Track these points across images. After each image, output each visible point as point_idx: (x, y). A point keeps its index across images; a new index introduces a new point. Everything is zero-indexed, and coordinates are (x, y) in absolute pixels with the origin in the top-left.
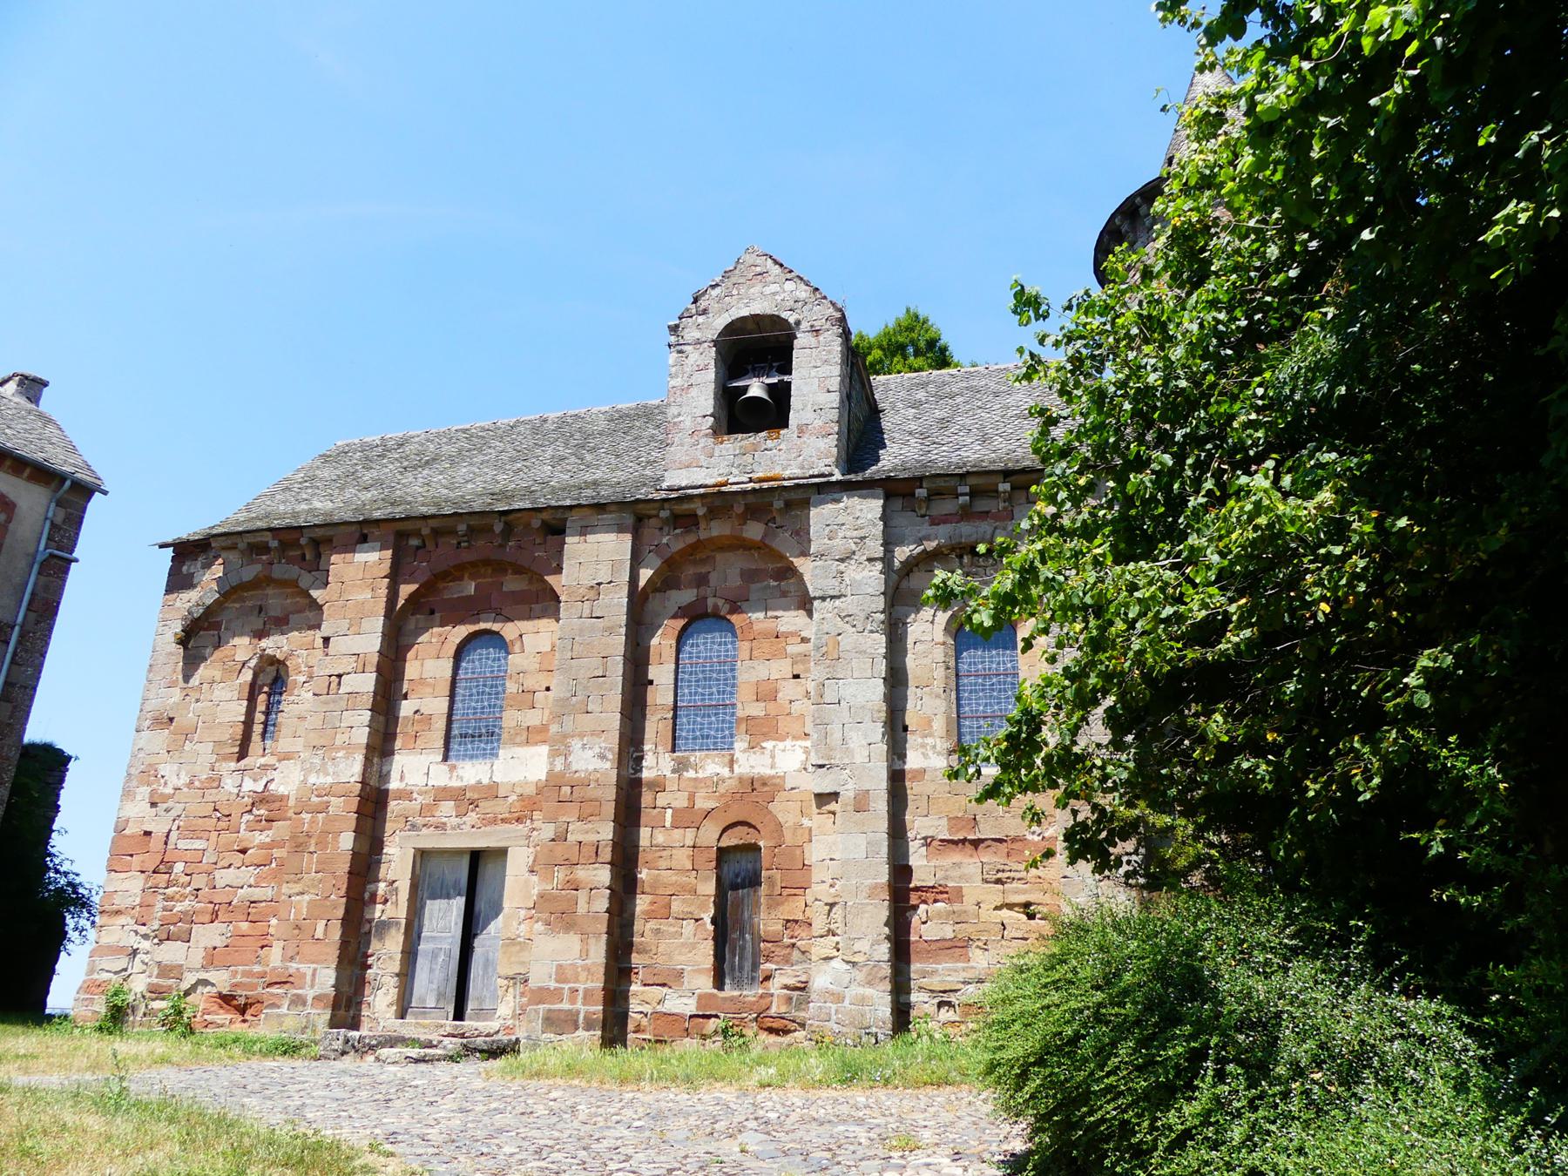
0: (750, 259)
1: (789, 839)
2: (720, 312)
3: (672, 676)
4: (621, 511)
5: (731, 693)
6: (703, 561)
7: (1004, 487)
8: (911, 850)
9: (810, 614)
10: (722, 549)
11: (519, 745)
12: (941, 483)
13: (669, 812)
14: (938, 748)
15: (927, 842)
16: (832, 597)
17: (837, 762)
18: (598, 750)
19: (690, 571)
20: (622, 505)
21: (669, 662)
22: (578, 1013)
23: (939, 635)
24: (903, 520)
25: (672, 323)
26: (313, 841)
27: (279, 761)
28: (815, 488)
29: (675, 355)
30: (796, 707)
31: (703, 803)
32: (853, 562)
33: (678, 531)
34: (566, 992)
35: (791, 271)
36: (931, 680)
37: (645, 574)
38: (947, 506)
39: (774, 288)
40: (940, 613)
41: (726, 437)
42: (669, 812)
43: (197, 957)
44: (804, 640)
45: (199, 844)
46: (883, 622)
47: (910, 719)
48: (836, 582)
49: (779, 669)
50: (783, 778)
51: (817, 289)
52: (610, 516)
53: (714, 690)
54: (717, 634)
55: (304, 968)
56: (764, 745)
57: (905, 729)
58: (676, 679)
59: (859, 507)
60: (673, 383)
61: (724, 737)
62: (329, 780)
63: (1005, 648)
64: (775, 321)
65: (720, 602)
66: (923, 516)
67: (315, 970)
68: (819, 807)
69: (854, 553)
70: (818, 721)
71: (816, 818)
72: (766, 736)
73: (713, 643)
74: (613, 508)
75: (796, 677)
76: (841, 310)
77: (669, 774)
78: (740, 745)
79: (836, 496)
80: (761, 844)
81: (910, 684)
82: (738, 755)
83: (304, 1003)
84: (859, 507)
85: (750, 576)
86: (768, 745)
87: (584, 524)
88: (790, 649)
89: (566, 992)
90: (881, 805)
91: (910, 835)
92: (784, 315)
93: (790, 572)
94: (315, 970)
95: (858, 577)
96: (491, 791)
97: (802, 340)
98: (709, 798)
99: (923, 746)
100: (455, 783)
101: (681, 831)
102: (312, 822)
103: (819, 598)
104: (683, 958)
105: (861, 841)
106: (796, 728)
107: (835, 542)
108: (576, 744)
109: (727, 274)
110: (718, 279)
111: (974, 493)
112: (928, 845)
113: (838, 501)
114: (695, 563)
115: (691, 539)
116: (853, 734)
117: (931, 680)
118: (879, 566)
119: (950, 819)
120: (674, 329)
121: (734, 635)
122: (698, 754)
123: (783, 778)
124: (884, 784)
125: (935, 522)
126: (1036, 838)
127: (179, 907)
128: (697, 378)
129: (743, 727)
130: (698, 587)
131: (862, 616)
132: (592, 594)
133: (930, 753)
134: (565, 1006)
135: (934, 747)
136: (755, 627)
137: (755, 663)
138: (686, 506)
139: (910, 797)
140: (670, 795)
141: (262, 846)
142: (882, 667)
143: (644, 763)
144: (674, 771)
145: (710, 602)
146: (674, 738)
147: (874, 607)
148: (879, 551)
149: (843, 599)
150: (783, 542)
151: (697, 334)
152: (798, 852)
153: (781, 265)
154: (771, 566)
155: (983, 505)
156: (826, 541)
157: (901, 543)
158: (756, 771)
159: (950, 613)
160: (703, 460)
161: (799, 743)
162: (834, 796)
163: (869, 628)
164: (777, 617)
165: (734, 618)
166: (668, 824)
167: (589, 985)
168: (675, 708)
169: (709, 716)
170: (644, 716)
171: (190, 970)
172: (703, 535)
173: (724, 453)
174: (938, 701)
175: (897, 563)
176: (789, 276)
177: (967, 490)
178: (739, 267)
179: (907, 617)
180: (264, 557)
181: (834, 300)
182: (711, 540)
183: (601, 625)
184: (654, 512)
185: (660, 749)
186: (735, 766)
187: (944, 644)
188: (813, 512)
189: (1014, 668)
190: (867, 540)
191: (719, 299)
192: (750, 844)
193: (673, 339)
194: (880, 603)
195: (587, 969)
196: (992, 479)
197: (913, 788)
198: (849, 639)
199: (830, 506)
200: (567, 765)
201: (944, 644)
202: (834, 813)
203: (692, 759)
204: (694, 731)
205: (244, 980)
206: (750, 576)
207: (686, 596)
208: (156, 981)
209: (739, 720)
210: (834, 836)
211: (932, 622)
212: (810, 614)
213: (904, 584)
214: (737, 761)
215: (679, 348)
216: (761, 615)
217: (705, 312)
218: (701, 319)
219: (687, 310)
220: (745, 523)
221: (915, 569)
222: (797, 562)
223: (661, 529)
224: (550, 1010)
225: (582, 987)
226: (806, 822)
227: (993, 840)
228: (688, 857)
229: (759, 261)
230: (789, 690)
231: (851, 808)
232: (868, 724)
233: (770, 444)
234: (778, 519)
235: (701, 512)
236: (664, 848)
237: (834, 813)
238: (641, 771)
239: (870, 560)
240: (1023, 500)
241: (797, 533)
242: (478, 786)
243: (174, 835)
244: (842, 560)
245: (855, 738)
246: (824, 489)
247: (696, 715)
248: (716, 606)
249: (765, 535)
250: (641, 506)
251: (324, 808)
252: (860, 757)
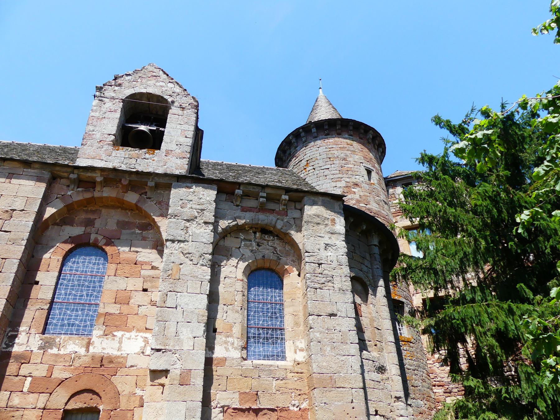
0: (151, 68)
1: (123, 404)
2: (129, 88)
3: (54, 280)
4: (41, 168)
5: (97, 297)
6: (93, 212)
7: (285, 197)
8: (213, 415)
9: (161, 253)
10: (107, 207)
12: (251, 188)
13: (29, 379)
14: (235, 345)
15: (224, 409)
16: (179, 241)
17: (170, 348)
19: (82, 216)
20: (44, 165)
21: (54, 271)
23: (240, 275)
24: (226, 206)
25: (99, 86)
28: (176, 179)
29: (97, 101)
30: (142, 310)
31: (59, 374)
32: (195, 223)
33: (80, 189)
35: (172, 79)
36: (234, 301)
37: (50, 211)
38: (252, 203)
39: (161, 84)
40: (241, 263)
41: (121, 148)
42: (29, 379)
44: (153, 268)
46: (210, 260)
47: (219, 324)
48: (183, 233)
49: (135, 284)
50: (126, 358)
51: (186, 90)
52: (33, 171)
53: (85, 293)
54: (93, 258)
56: (115, 333)
57: (215, 330)
58: (57, 283)
59: (202, 193)
60: (93, 114)
61: (85, 326)
63: (276, 288)
64: (160, 99)
66: (237, 206)
68: (152, 380)
69: (196, 217)
70: (160, 319)
71: (149, 389)
72: (118, 328)
73: (90, 263)
74: (37, 166)
75: (145, 290)
76: (197, 102)
77: (35, 350)
78: (97, 332)
79: (189, 185)
80: (101, 407)
81: (220, 302)
82: (94, 339)
84: (202, 193)
85: (123, 225)
86: (119, 334)
88: (143, 272)
90: (199, 382)
91: (213, 404)
92: (166, 97)
93: (152, 226)
95: (198, 232)
97: (174, 110)
98: (65, 370)
99: (226, 343)
101: (36, 395)
103: (170, 240)
105: (182, 407)
106: (141, 324)
107: (185, 210)
109: (136, 72)
110: (130, 72)
111: (269, 199)
112: (224, 412)
113: (190, 188)
114: (87, 212)
115: (88, 195)
116: (184, 330)
117: (234, 301)
118: (211, 227)
119: (241, 394)
120: (99, 89)
121: (106, 259)
122: (63, 336)
123: (126, 358)
124: (202, 366)
125: (244, 210)
126: (296, 409)
128: (108, 115)
129: (102, 320)
130: (86, 226)
131: (198, 254)
132: (6, 216)
133: (230, 348)
135: (233, 344)
136: (121, 256)
137: (117, 279)
138: (89, 174)
139: (215, 377)
140: (34, 366)
142: (207, 288)
143: (17, 341)
144: (40, 348)
145: (93, 237)
146: (46, 324)
147: (205, 251)
148: (212, 220)
149: (186, 243)
150: (149, 207)
151: (113, 94)
152: (129, 414)
153: (168, 75)
154: (138, 221)
155: (271, 206)
156: (179, 208)
157: (223, 218)
158: (106, 351)
159: (247, 263)
160: (104, 157)
161: (141, 334)
162: (165, 372)
163: (201, 262)
164: (137, 252)
165: (108, 249)
166: (25, 390)
168: (52, 302)
169: (77, 310)
170: (25, 306)
172: (97, 194)
173: (118, 155)
174: (237, 315)
175: (220, 229)
176: (171, 81)
177: (265, 195)
178: (144, 70)
179: (221, 262)
181: (194, 96)
182: (101, 198)
183: (7, 237)
184: (66, 174)
185: (33, 331)
186: (91, 348)
187: (242, 280)
188: (173, 191)
189: (280, 300)
190: (205, 212)
191: (130, 81)
192: (92, 407)
193: (98, 94)
194: (210, 249)
196: (279, 192)
197: (217, 371)
198: (187, 268)
199: (184, 189)
201: (242, 280)
202: (163, 385)
203: (58, 340)
204: (63, 320)
206: (123, 225)
207: (77, 231)
209: (100, 315)
210: (162, 402)
211: (236, 267)
212: (161, 253)
213: (221, 243)
215: (101, 98)
216: (127, 249)
217: (120, 85)
218: (116, 88)
219: (110, 82)
220: (126, 192)
221: (229, 235)
222: (157, 219)
223: (68, 186)
226: (139, 392)
227: (269, 409)
229: (155, 70)
230: (139, 298)
231: (176, 382)
232: (194, 324)
233: (147, 156)
234: (149, 194)
235: (99, 179)
236: (18, 409)
237: (163, 385)
238: (12, 346)
239: (206, 223)
240: (293, 207)
241: (160, 203)
244: (188, 221)
245: (184, 333)
246: (180, 179)
247: (68, 309)
248: (96, 240)
249: (139, 201)
250: (58, 168)
252: (187, 345)
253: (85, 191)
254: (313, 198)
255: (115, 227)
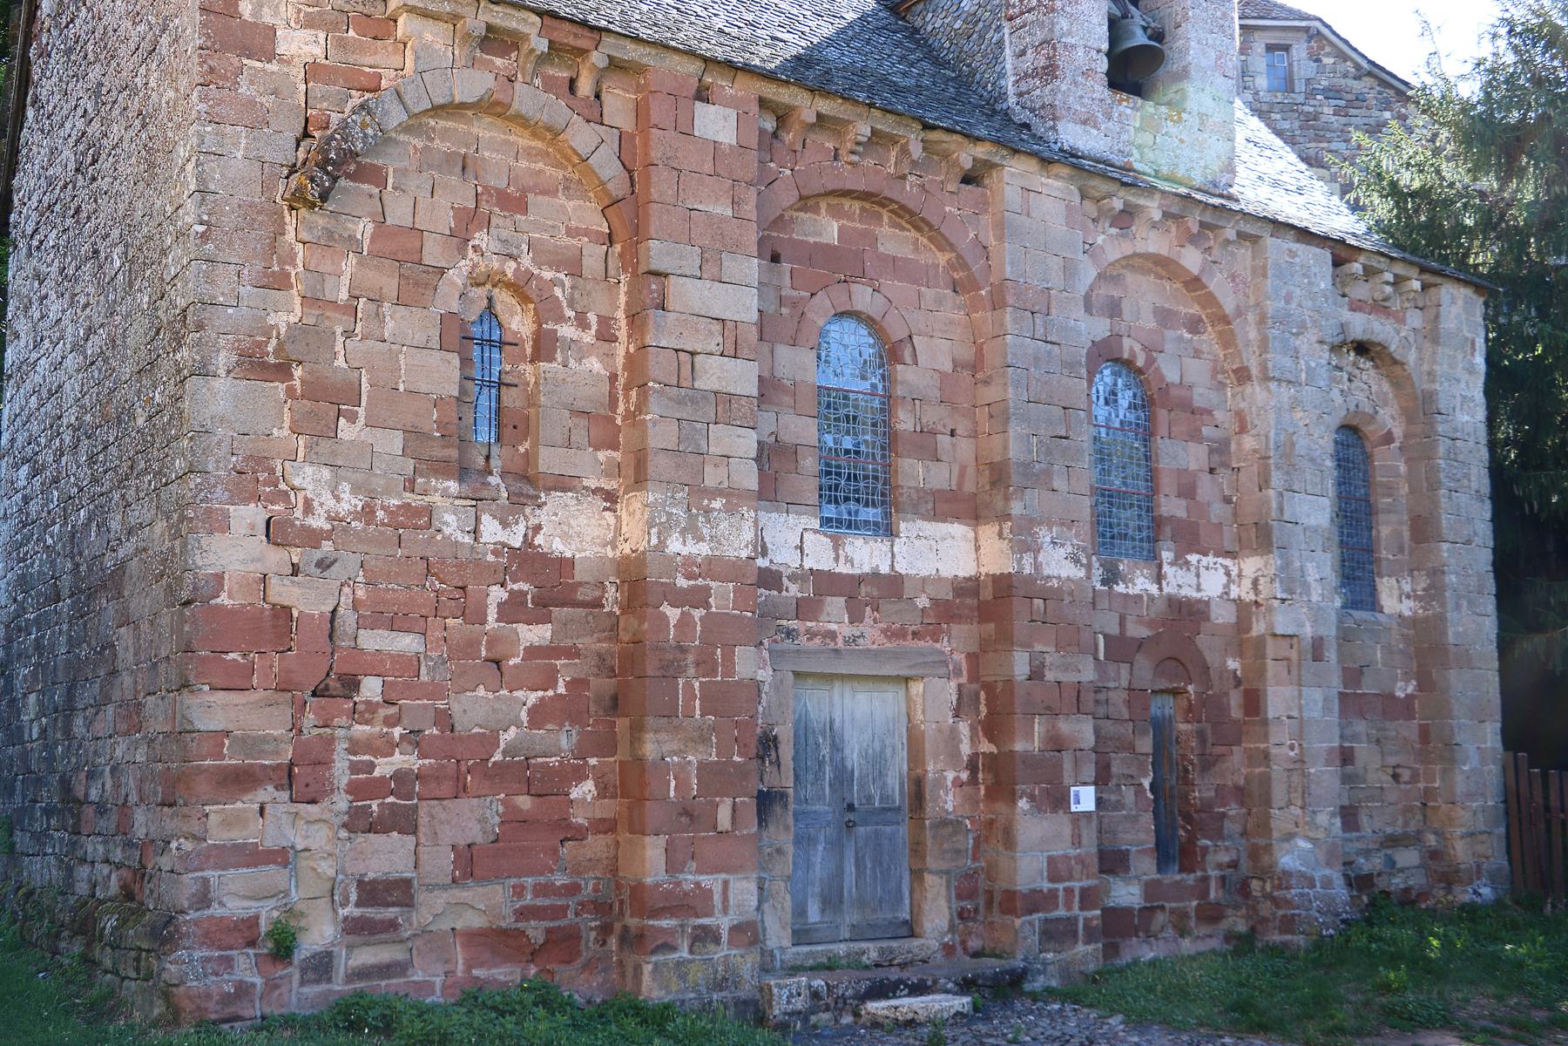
11: (925, 519)
18: (1070, 550)
22: (1076, 918)
26: (690, 658)
27: (548, 490)
31: (1137, 631)
34: (1061, 894)
43: (441, 862)
45: (407, 643)
55: (706, 880)
56: (1189, 557)
62: (704, 549)
65: (1137, 348)
67: (726, 883)
83: (717, 940)
86: (1193, 558)
87: (1026, 184)
89: (1061, 894)
94: (726, 883)
96: (892, 585)
100: (843, 569)
102: (685, 621)
104: (1127, 836)
108: (1044, 535)
127: (384, 767)
130: (1111, 317)
134: (1061, 912)
141: (532, 652)
152: (1225, 700)
158: (1184, 592)
161: (1220, 560)
167: (1087, 883)
171: (431, 888)
180: (499, 61)
186: (1164, 583)
195: (1080, 860)
200: (1037, 566)
205: (540, 902)
208: (357, 912)
214: (1165, 578)
224: (1046, 920)
225: (1077, 885)
228: (1124, 701)
234: (1216, 252)
242: (875, 575)
243: (347, 618)
245: (1310, 572)
251: (699, 598)
253: (1122, 236)
254: (1451, 290)
255: (1152, 325)
